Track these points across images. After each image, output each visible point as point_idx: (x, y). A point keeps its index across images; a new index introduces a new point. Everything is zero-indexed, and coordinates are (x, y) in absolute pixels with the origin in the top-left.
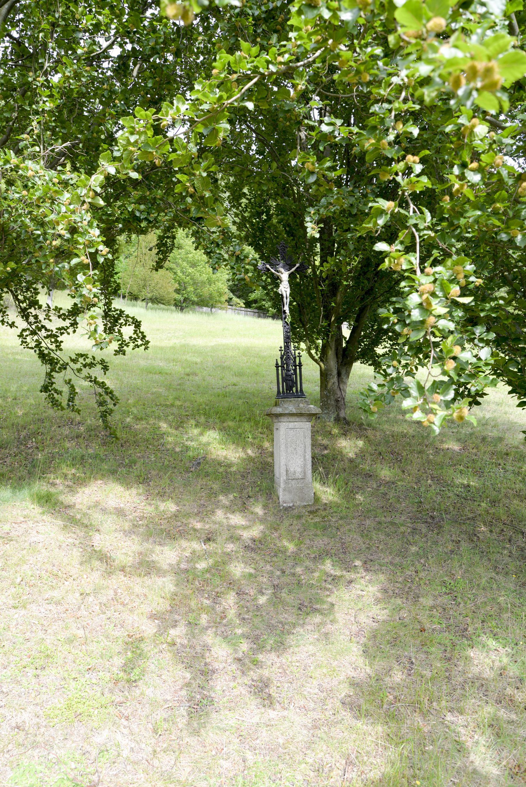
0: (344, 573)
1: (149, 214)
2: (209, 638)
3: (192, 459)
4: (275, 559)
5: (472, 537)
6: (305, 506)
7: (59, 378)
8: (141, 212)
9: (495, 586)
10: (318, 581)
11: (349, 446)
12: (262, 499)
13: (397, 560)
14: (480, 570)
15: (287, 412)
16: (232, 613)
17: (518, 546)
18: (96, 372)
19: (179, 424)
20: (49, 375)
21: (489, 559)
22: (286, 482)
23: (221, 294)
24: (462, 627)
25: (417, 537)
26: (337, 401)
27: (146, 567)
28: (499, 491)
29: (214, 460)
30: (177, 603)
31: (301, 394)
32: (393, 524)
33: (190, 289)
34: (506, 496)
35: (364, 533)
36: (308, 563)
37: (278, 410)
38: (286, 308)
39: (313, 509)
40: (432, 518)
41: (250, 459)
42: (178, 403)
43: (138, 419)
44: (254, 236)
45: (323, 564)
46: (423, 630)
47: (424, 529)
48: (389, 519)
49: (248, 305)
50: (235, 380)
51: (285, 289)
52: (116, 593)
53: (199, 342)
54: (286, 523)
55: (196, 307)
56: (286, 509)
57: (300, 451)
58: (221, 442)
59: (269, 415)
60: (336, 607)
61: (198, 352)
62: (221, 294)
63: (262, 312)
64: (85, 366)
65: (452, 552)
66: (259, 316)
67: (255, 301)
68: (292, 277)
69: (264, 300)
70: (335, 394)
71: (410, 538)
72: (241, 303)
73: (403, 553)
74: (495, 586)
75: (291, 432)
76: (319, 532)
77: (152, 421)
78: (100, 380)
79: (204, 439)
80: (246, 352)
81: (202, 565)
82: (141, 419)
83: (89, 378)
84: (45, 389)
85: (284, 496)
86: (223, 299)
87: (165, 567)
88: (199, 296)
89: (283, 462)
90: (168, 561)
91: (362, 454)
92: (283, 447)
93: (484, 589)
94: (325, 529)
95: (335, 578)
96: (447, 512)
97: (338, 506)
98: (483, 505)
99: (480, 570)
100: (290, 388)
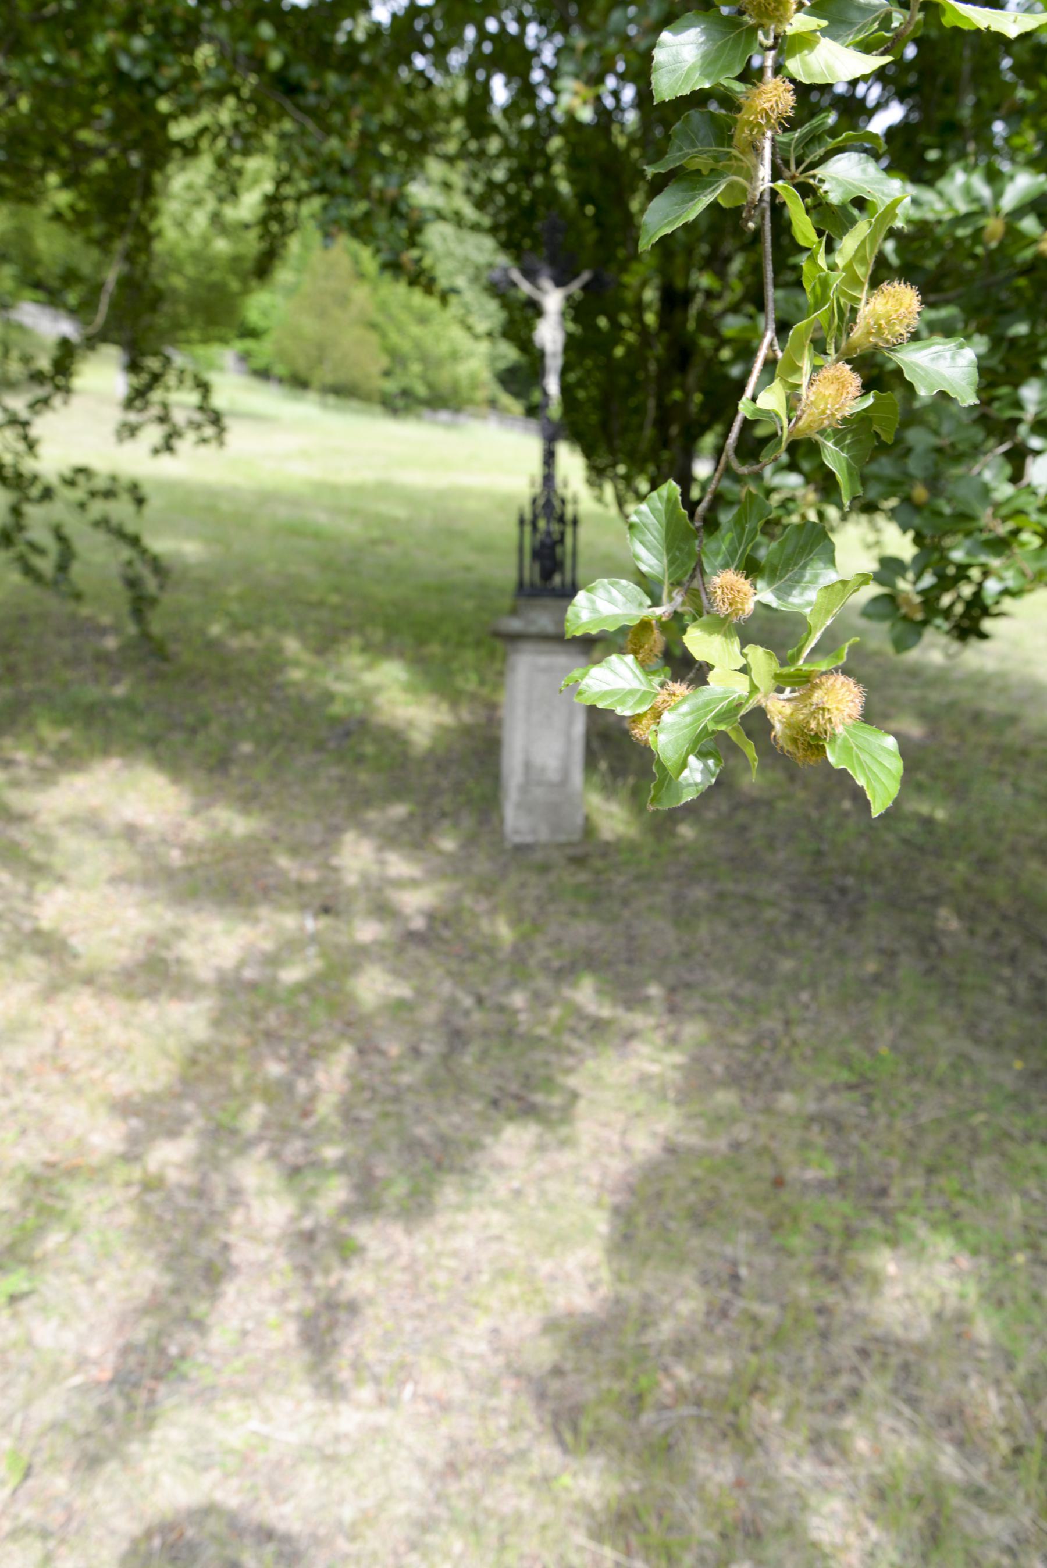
0: (620, 1012)
1: (157, 65)
2: (253, 1173)
3: (334, 721)
4: (469, 968)
5: (928, 941)
6: (561, 846)
8: (136, 59)
9: (967, 1079)
10: (557, 1030)
12: (468, 822)
13: (747, 990)
14: (935, 1031)
15: (533, 629)
16: (326, 1107)
17: (1032, 977)
18: (121, 510)
19: (326, 643)
20: (16, 511)
21: (961, 1006)
22: (524, 789)
24: (876, 1181)
25: (801, 936)
27: (154, 974)
28: (998, 837)
29: (384, 728)
30: (199, 1068)
32: (750, 899)
33: (416, 368)
34: (1014, 850)
35: (683, 916)
36: (543, 983)
37: (515, 625)
39: (579, 851)
40: (843, 891)
42: (334, 599)
43: (236, 628)
44: (511, 226)
45: (574, 985)
46: (779, 1182)
47: (818, 914)
48: (743, 888)
50: (471, 558)
51: (550, 334)
52: (58, 1043)
53: (416, 478)
54: (514, 879)
55: (426, 412)
56: (521, 849)
58: (410, 688)
59: (498, 635)
60: (582, 1105)
61: (409, 497)
64: (93, 494)
65: (876, 978)
71: (786, 939)
72: (516, 407)
73: (762, 975)
74: (967, 1079)
76: (582, 907)
77: (268, 631)
78: (130, 528)
79: (369, 678)
81: (292, 975)
82: (247, 627)
83: (103, 523)
85: (516, 821)
86: (481, 395)
87: (205, 974)
88: (430, 386)
90: (216, 961)
93: (940, 1084)
94: (595, 900)
95: (598, 1027)
96: (875, 878)
97: (633, 848)
98: (961, 866)
99: (935, 1031)
100: (547, 575)
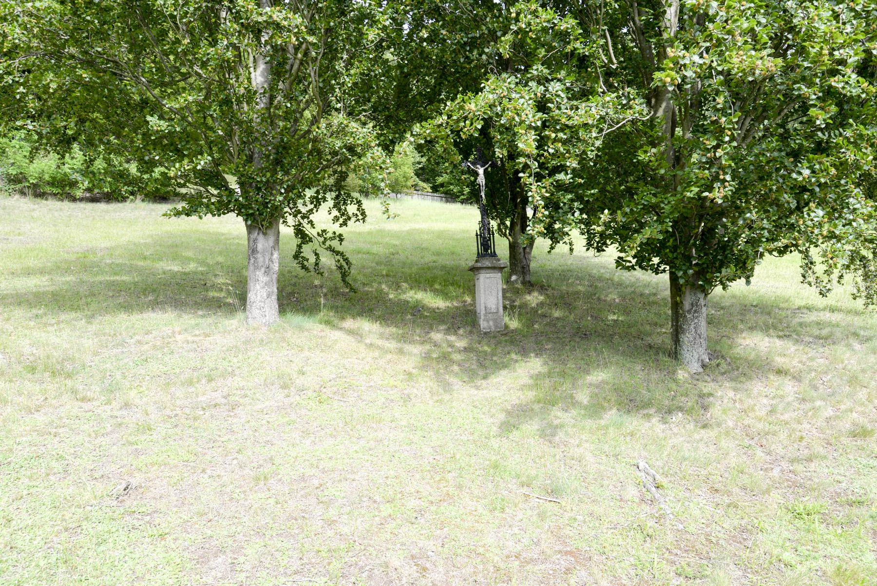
7: (307, 250)
11: (534, 299)
20: (300, 246)
22: (485, 315)
23: (407, 179)
26: (523, 268)
31: (494, 255)
37: (479, 265)
38: (483, 194)
41: (457, 308)
49: (435, 189)
50: (435, 258)
51: (481, 180)
56: (485, 333)
57: (494, 293)
62: (407, 179)
63: (451, 197)
66: (447, 201)
67: (442, 185)
68: (485, 171)
69: (451, 184)
70: (521, 262)
72: (427, 186)
75: (488, 281)
77: (375, 285)
80: (440, 234)
84: (296, 257)
85: (483, 324)
89: (482, 302)
91: (541, 304)
92: (482, 291)
100: (486, 250)
